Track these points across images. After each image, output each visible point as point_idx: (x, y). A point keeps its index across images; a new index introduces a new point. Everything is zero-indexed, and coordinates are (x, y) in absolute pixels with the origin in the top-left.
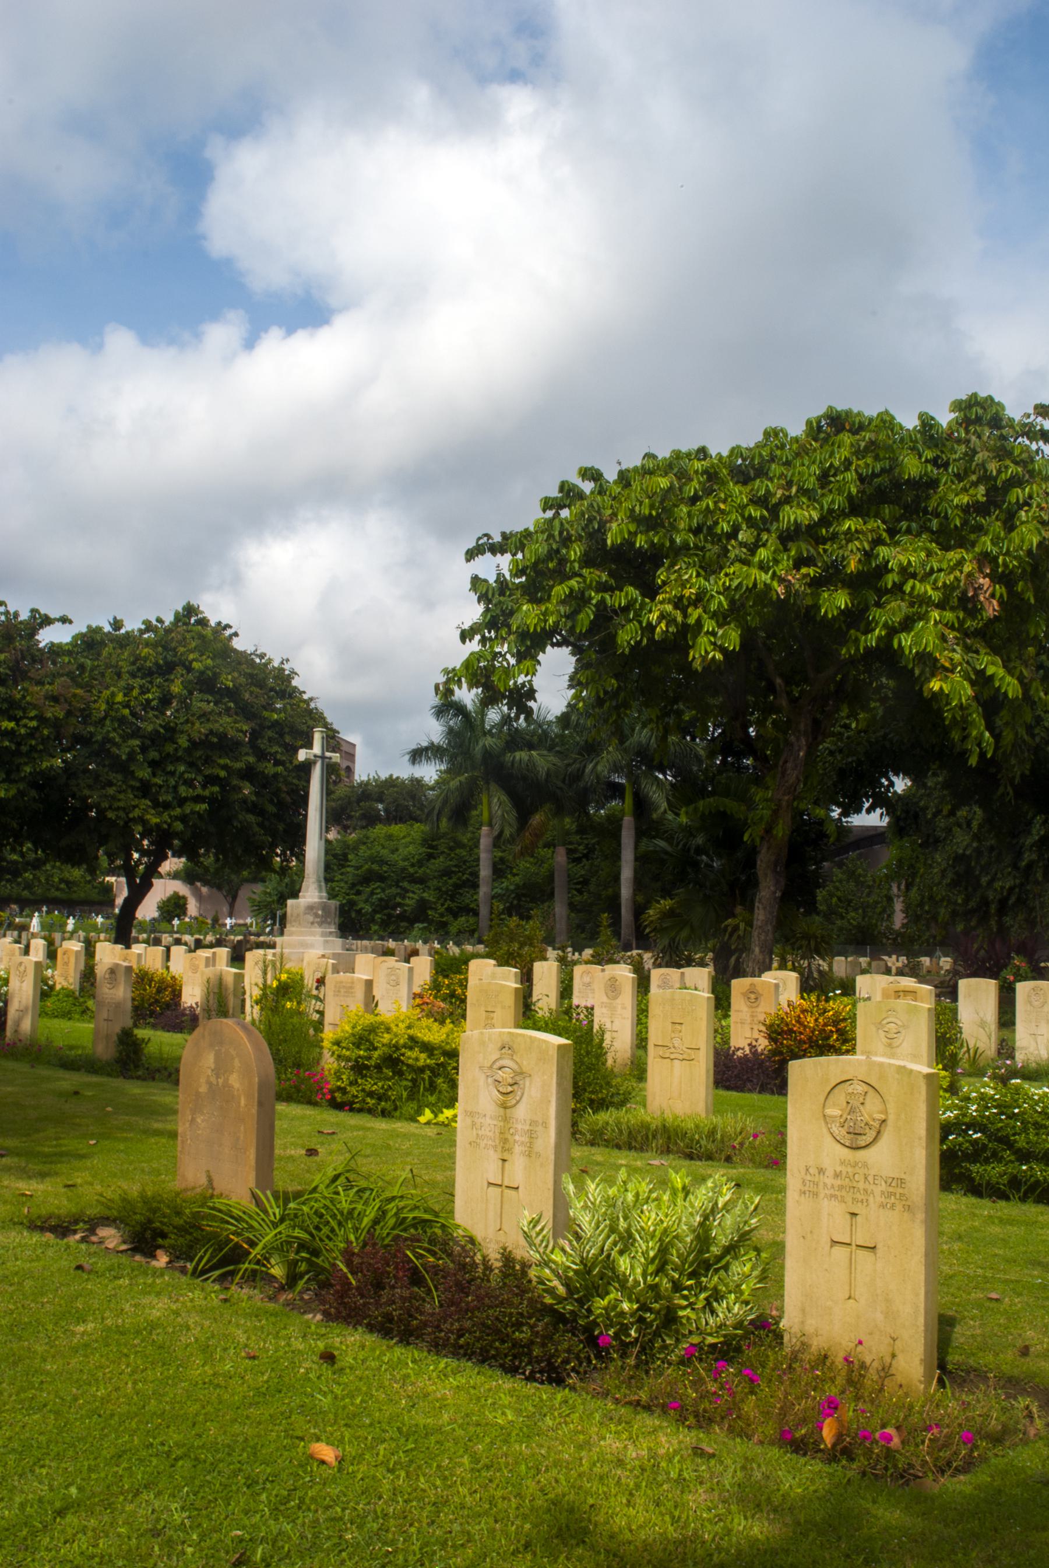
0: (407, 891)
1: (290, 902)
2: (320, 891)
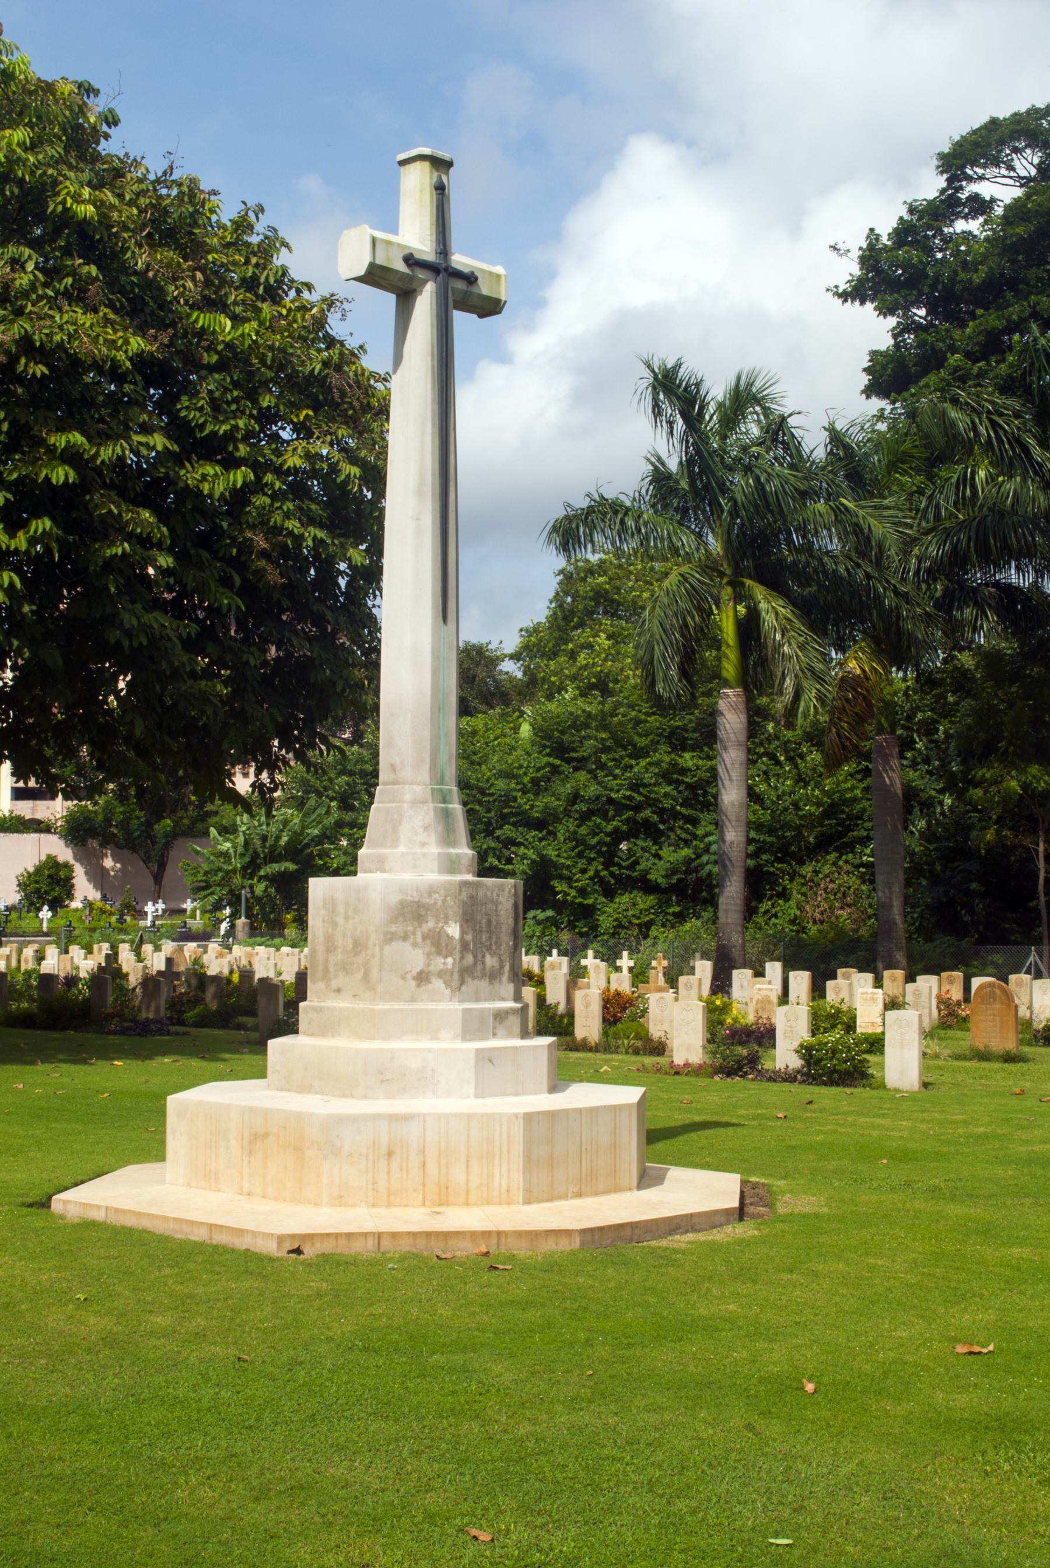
0: (513, 842)
1: (318, 887)
2: (448, 838)
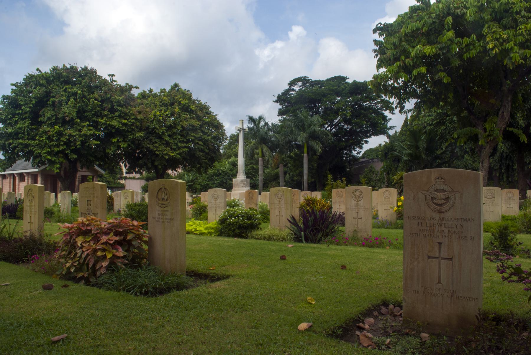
1: (234, 180)
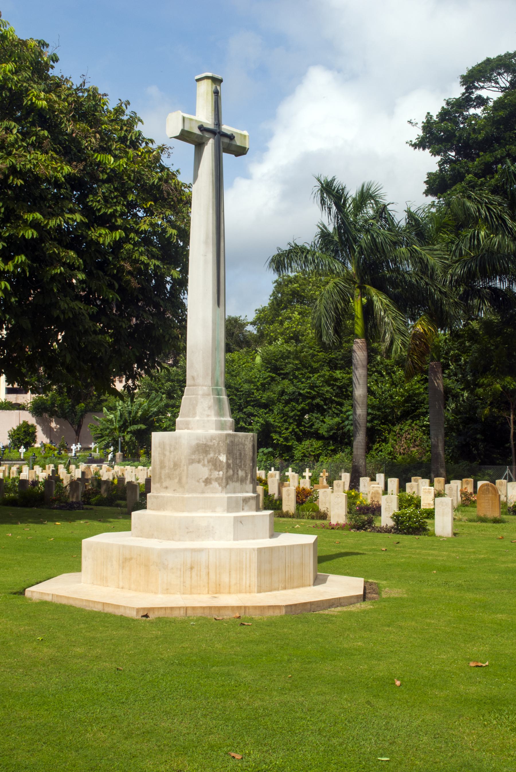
0: (252, 415)
1: (156, 437)
2: (220, 413)
